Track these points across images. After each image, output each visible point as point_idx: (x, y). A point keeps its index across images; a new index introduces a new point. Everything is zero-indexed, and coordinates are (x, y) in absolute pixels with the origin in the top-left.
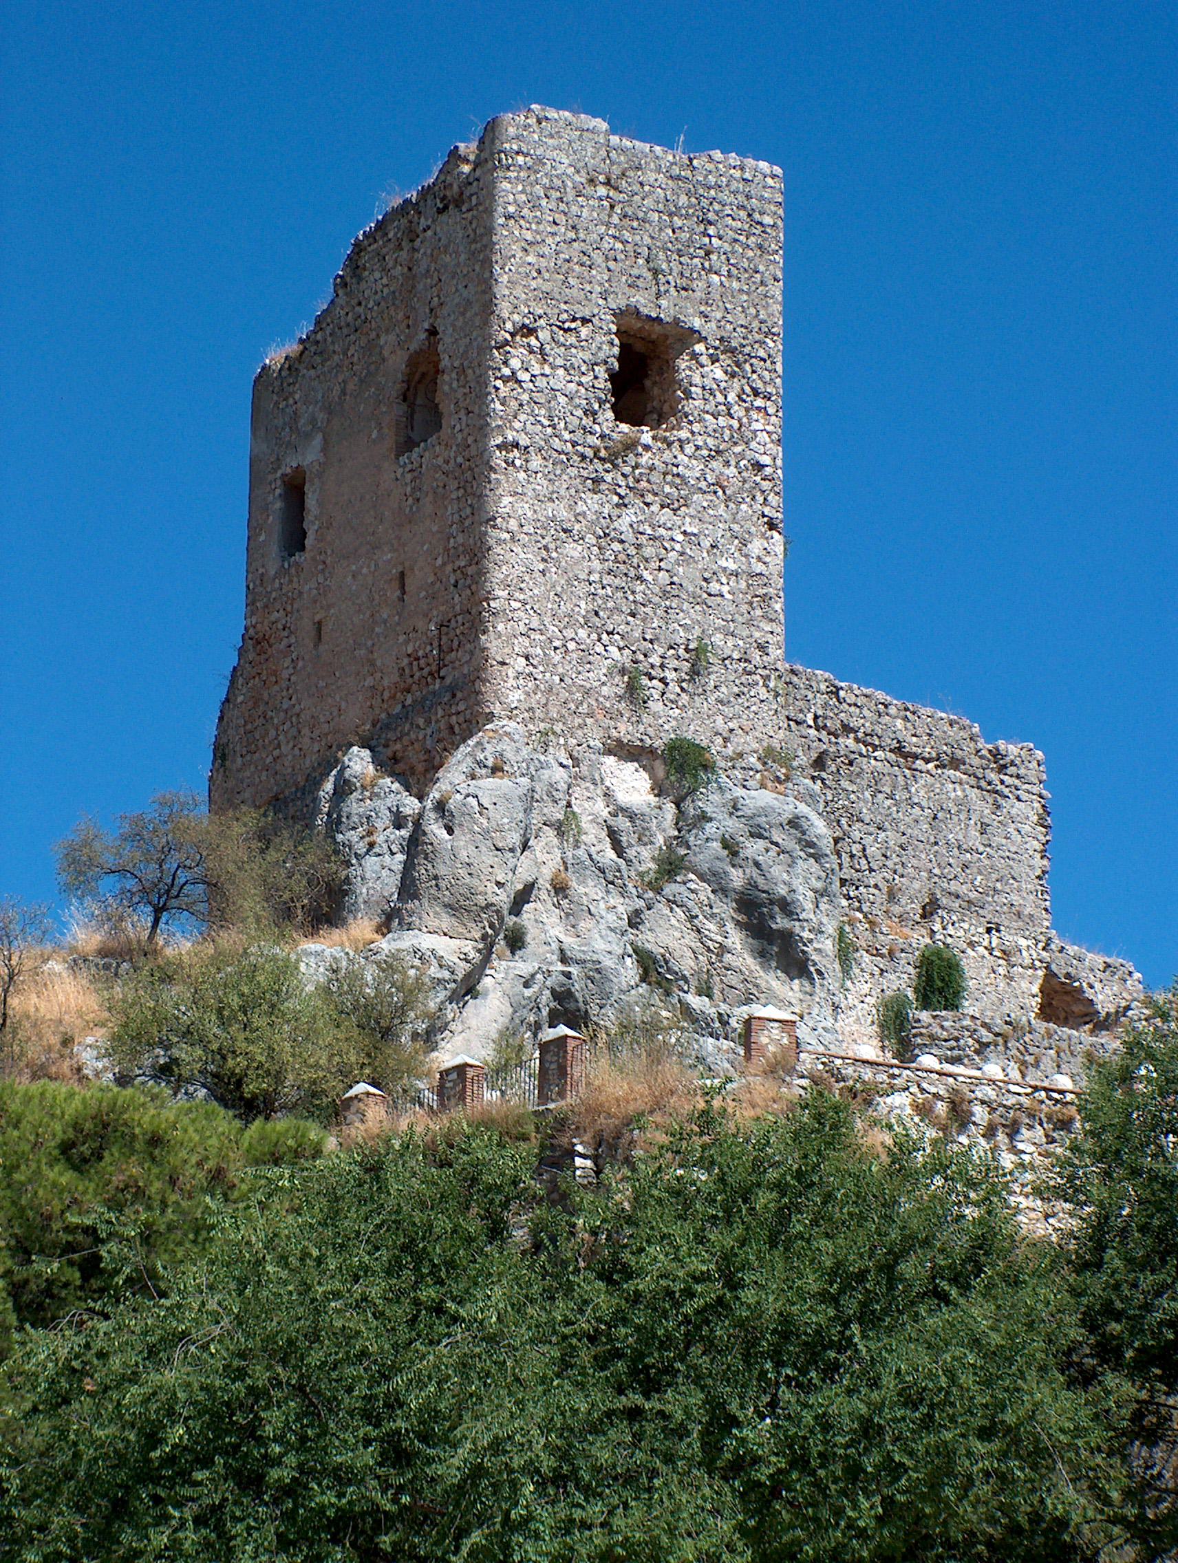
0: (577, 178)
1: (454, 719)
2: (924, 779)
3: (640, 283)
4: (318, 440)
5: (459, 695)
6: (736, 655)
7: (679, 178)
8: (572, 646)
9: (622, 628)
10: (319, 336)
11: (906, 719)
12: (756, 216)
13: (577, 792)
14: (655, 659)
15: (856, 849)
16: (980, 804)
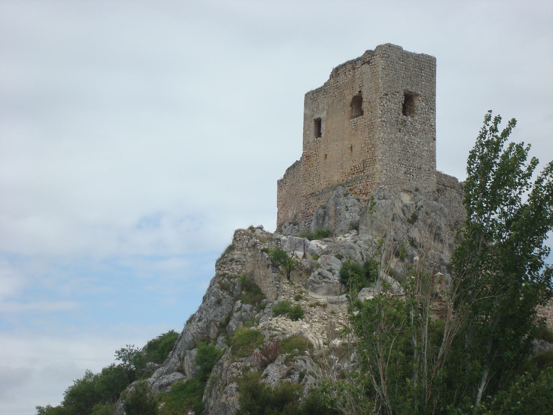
2: (448, 192)
4: (325, 112)
8: (395, 167)
9: (405, 163)
14: (411, 171)
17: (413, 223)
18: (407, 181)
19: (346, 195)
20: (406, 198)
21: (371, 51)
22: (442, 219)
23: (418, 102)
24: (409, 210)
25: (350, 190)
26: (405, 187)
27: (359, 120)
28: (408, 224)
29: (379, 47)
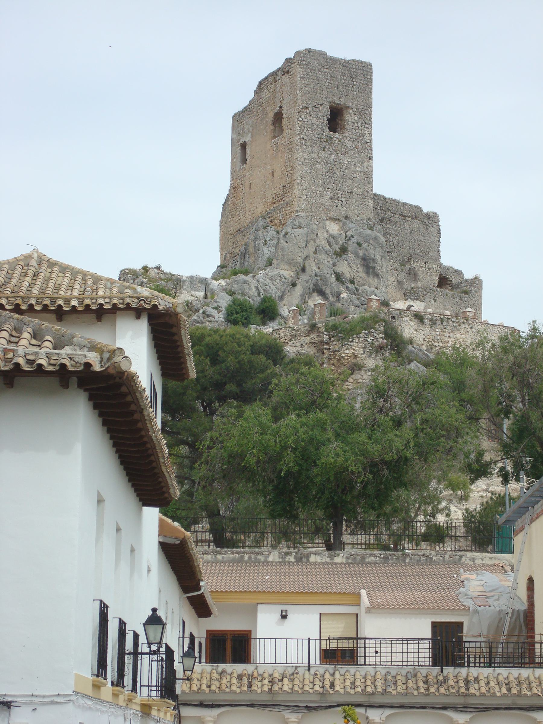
0: (319, 67)
1: (287, 212)
3: (336, 94)
4: (250, 135)
5: (289, 205)
6: (360, 194)
7: (345, 66)
8: (318, 192)
9: (331, 187)
10: (250, 107)
11: (404, 207)
12: (366, 76)
13: (319, 231)
15: (391, 243)
16: (423, 229)
17: (341, 256)
18: (335, 208)
19: (265, 228)
20: (334, 228)
21: (290, 59)
22: (377, 250)
23: (349, 115)
24: (337, 242)
25: (271, 221)
26: (331, 214)
27: (280, 141)
28: (334, 256)
29: (298, 53)
